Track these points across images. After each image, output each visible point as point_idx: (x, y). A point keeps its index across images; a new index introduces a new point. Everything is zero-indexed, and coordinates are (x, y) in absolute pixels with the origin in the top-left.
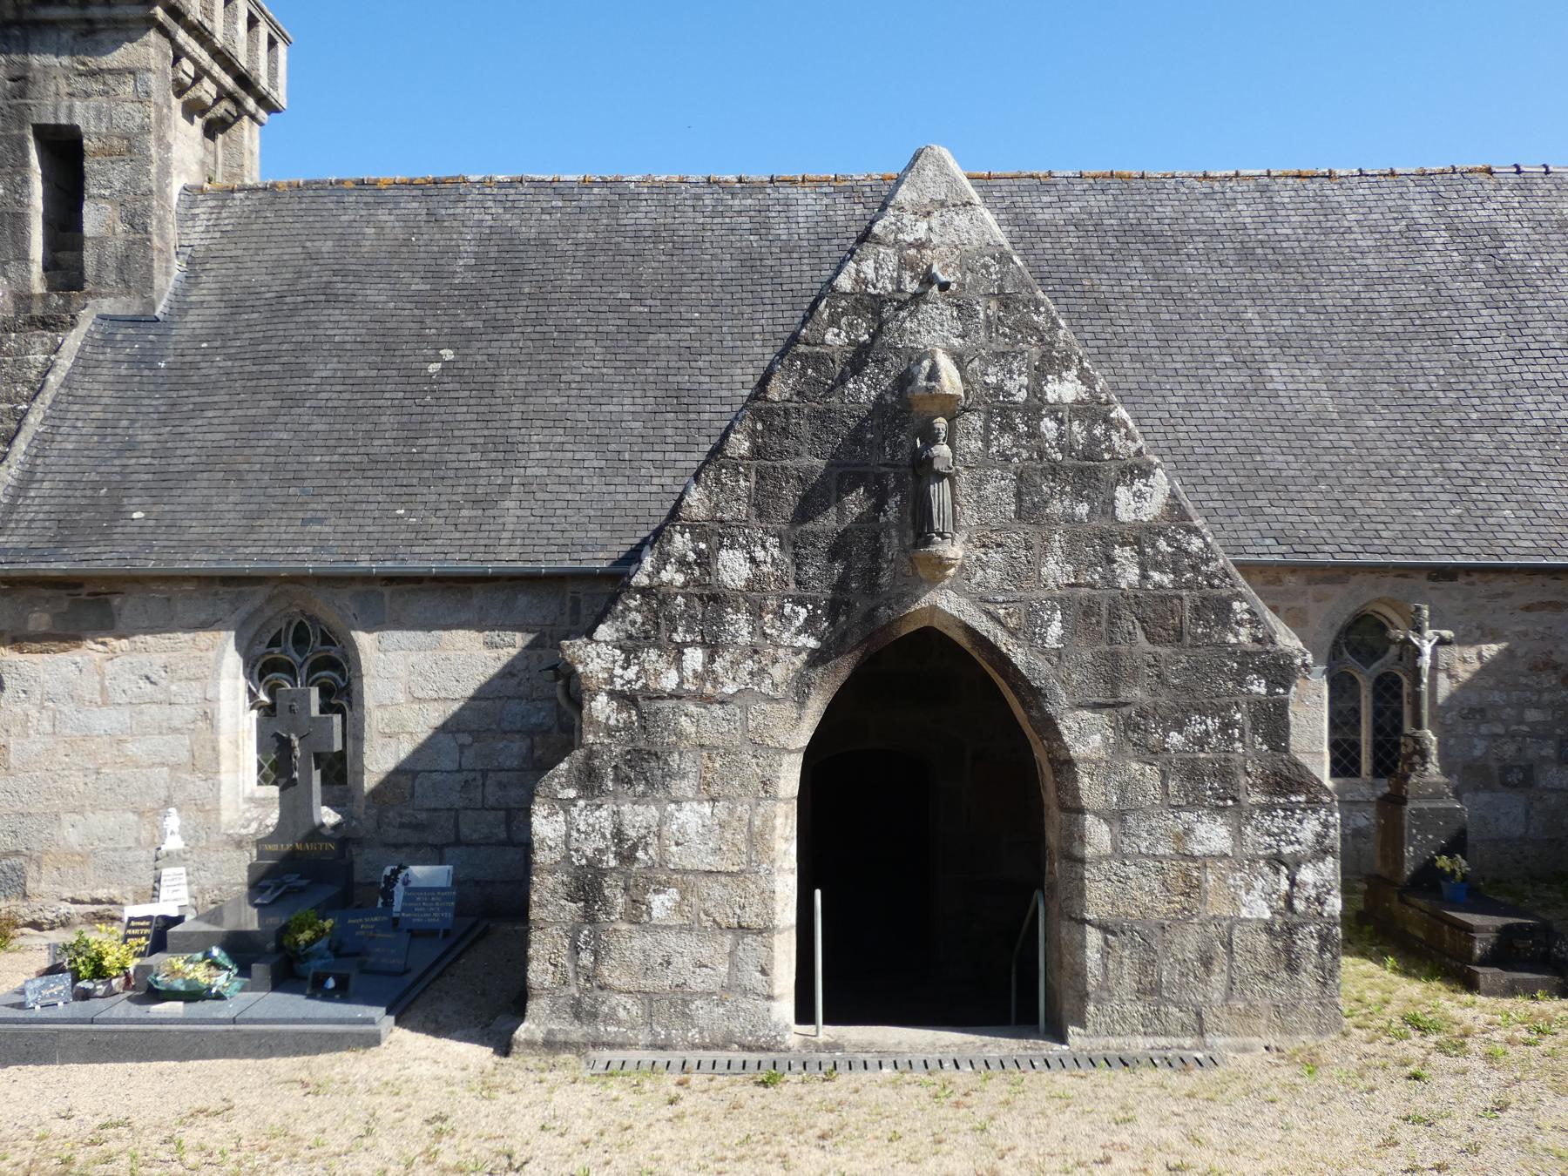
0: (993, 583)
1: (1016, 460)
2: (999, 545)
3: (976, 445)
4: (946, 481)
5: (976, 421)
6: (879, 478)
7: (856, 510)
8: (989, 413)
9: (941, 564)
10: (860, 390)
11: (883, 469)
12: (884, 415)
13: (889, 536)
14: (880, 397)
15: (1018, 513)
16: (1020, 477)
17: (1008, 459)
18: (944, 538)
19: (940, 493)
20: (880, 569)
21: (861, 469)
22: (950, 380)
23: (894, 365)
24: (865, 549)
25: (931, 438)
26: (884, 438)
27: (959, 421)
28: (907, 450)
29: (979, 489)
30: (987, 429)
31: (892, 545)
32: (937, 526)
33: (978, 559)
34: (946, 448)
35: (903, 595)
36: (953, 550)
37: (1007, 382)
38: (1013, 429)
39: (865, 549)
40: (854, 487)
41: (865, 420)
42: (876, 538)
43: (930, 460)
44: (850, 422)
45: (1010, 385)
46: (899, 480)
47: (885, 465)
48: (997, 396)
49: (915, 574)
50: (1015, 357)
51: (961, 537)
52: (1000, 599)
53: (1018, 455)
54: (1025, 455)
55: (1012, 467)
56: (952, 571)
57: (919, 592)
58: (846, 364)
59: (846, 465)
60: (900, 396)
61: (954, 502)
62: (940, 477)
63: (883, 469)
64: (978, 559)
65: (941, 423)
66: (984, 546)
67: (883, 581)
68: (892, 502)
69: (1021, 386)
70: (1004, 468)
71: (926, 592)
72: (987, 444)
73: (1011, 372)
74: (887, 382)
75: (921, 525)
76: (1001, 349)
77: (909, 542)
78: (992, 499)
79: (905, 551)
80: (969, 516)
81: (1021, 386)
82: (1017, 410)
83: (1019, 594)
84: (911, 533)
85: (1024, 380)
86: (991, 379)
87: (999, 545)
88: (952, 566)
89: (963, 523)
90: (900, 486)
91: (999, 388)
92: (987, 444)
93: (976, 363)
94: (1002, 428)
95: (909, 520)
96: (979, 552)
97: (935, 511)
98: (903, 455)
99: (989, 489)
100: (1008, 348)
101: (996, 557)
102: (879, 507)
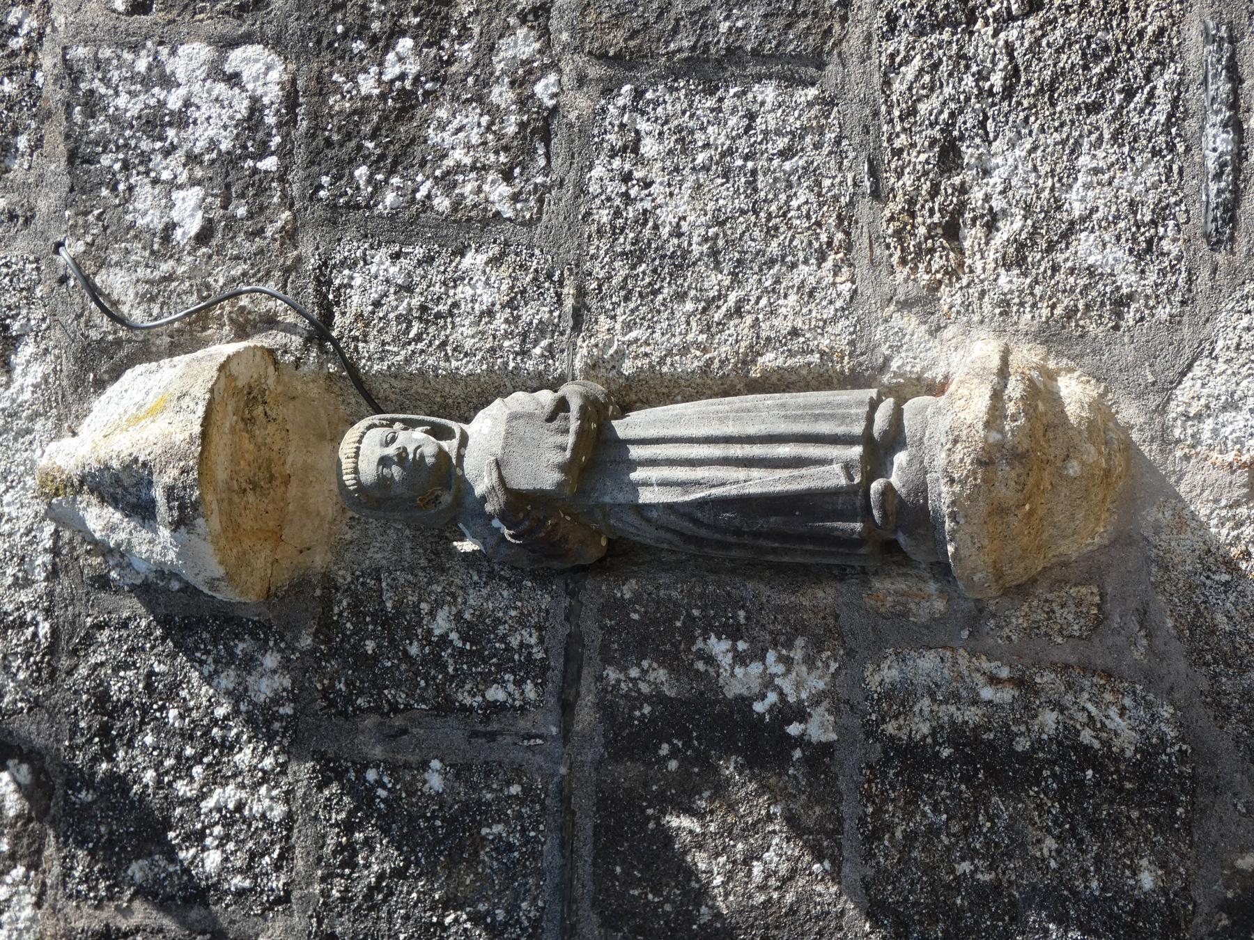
0: (1142, 180)
1: (544, 89)
2: (949, 156)
3: (480, 280)
4: (625, 427)
5: (371, 280)
6: (629, 737)
7: (779, 852)
8: (335, 216)
9: (1027, 447)
10: (233, 817)
11: (586, 716)
12: (341, 709)
13: (899, 698)
14: (262, 722)
15: (795, 68)
16: (623, 62)
17: (541, 126)
18: (895, 438)
19: (681, 454)
20: (1067, 748)
21: (586, 824)
22: (151, 413)
23: (129, 654)
24: (966, 813)
25: (429, 494)
26: (446, 707)
27: (373, 358)
28: (494, 600)
29: (681, 262)
30: (404, 227)
31: (944, 683)
32: (830, 474)
33: (1016, 258)
34: (485, 431)
35: (1197, 631)
36: (960, 380)
37: (200, 137)
38: (404, 103)
39: (966, 813)
40: (665, 860)
41: (364, 798)
42: (912, 759)
43: (520, 504)
44: (376, 863)
45: (213, 128)
46: (642, 642)
47: (567, 708)
48: (260, 184)
49: (1092, 571)
50: (92, 104)
51: (910, 345)
52: (1217, 142)
53: (523, 77)
54: (521, 45)
55: (579, 104)
56: (1074, 392)
57: (1182, 549)
58: (115, 875)
59: (564, 892)
60: (261, 632)
61: (739, 381)
62: (599, 453)
63: (586, 716)
64: (1016, 258)
65: (366, 449)
66: (952, 231)
67: (1125, 733)
68: (740, 680)
69: (217, 72)
70: (585, 139)
71: (1184, 520)
72: (474, 224)
73: (153, 123)
74: (197, 690)
75: (820, 547)
76: (56, 167)
77: (932, 602)
78: (726, 197)
79: (977, 616)
80: (802, 308)
81: (217, 72)
82: (322, 87)
83: (1196, 50)
84: (888, 588)
85: (190, 58)
86: (189, 208)
87: (949, 156)
88: (1040, 393)
89: (837, 337)
90: (662, 638)
91: (226, 173)
92: (474, 224)
93: (116, 282)
94: (400, 157)
95: (824, 595)
96: (983, 252)
97: (759, 482)
98: (524, 617)
99: (678, 209)
100: (54, 135)
101: (1005, 168)
102: (762, 740)
